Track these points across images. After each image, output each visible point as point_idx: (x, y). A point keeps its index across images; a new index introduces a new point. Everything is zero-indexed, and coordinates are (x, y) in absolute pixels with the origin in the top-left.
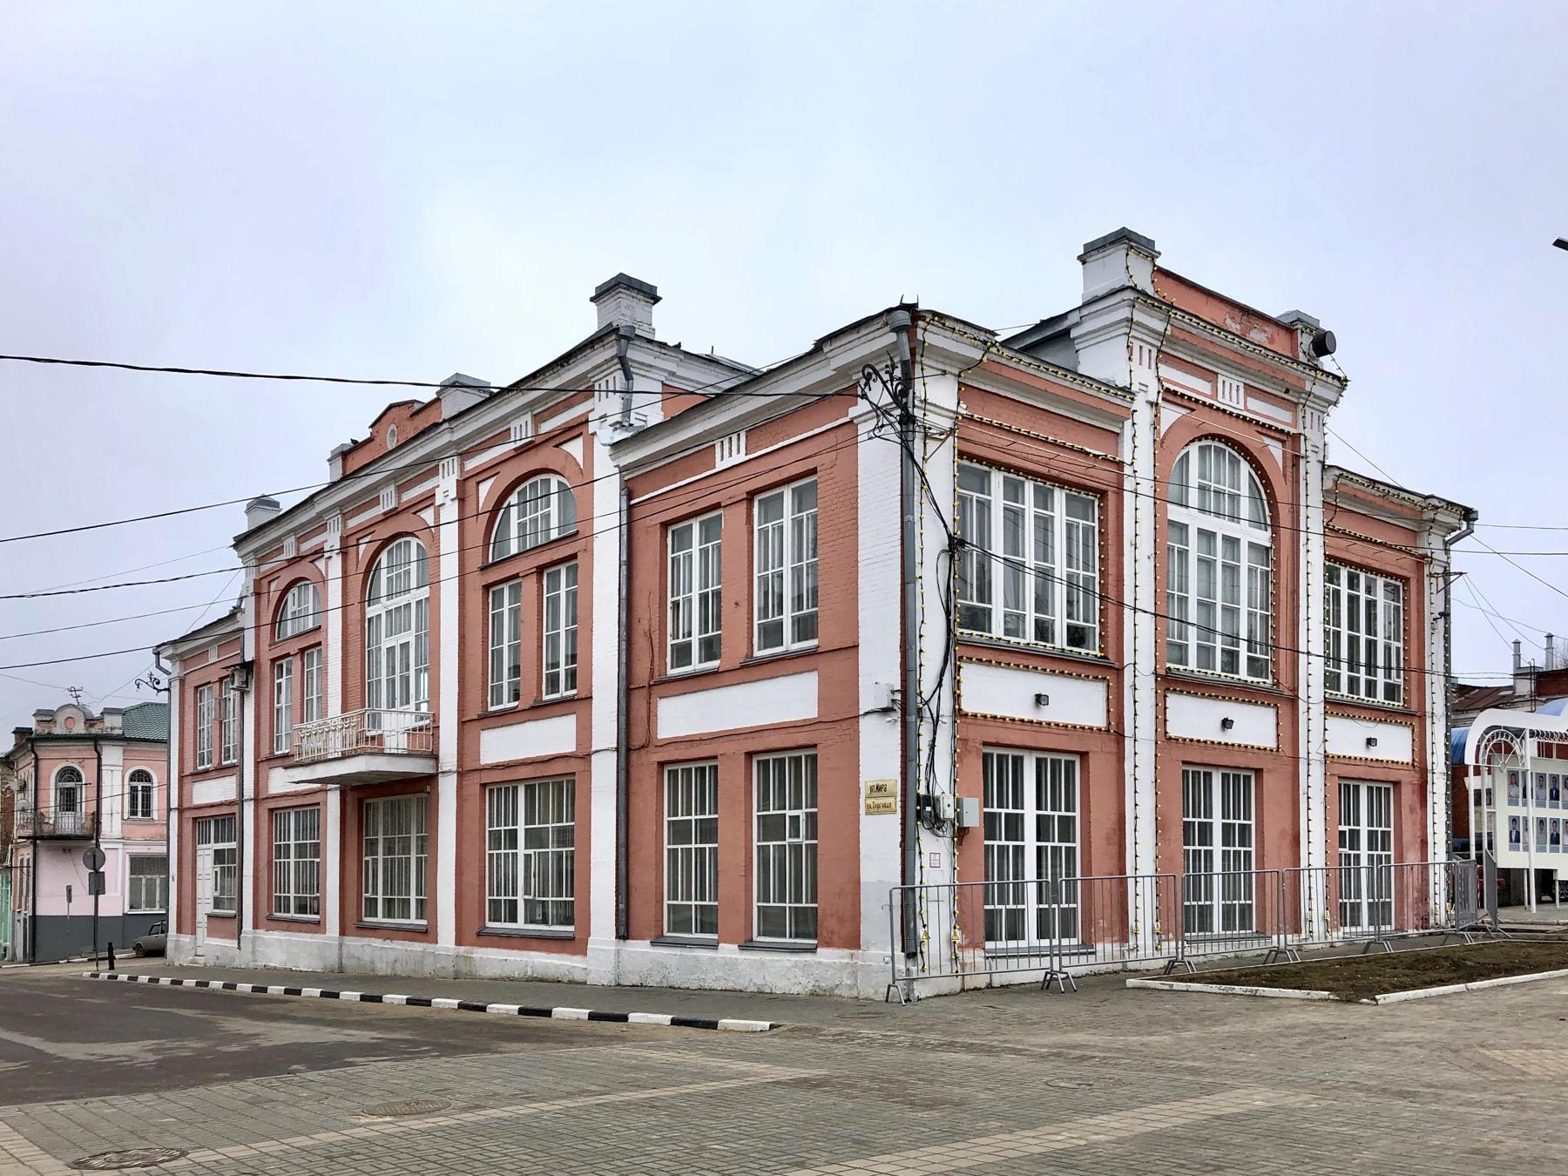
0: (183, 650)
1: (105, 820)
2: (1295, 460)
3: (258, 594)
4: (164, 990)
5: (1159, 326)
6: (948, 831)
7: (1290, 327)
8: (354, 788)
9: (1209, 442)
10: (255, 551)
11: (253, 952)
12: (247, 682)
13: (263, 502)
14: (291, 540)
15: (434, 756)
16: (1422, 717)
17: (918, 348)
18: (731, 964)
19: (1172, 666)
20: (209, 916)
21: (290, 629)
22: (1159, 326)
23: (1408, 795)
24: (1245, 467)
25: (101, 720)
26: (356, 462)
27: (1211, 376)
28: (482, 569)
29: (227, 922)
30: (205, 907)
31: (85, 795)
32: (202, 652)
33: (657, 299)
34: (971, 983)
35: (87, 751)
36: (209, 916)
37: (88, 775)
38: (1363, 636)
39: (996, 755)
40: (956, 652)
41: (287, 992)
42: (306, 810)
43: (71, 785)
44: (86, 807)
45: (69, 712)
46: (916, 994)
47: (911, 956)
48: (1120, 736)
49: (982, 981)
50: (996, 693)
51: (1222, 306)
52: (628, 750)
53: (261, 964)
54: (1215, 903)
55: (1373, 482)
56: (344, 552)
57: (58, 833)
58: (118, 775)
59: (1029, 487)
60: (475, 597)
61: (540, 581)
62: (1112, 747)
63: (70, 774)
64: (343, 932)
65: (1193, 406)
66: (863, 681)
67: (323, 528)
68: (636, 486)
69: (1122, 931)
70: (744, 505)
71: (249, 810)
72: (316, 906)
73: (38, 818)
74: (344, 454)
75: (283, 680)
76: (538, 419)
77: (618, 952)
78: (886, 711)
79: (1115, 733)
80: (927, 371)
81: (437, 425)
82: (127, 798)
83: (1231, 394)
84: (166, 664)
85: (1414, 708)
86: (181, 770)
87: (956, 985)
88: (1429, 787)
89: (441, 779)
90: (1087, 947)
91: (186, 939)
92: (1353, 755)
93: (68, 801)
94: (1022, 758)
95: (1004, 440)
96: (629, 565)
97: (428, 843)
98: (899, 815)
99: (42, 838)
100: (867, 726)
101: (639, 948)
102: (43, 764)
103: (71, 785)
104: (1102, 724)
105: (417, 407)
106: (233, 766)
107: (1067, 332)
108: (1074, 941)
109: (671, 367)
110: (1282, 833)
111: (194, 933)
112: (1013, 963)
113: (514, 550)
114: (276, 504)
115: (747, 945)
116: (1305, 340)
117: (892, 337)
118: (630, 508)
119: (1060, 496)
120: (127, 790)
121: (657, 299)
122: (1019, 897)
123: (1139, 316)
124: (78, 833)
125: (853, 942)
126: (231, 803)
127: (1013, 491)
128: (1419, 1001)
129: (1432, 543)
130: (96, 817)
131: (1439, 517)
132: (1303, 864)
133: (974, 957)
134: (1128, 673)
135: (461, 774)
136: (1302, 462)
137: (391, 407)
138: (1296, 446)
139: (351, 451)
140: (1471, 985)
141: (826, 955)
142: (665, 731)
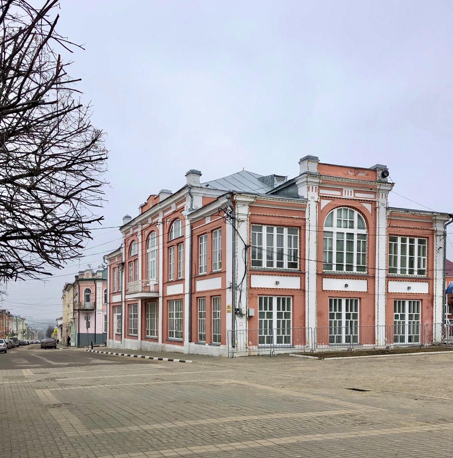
0: (110, 257)
1: (97, 305)
2: (375, 209)
3: (125, 243)
4: (100, 355)
5: (318, 181)
6: (244, 317)
7: (374, 170)
8: (144, 300)
9: (341, 208)
10: (124, 231)
11: (124, 345)
12: (123, 268)
13: (127, 217)
14: (131, 230)
15: (158, 292)
16: (433, 279)
17: (234, 202)
18: (207, 348)
19: (324, 271)
20: (116, 334)
21: (132, 254)
22: (318, 181)
23: (425, 303)
24: (356, 213)
25: (96, 274)
26: (145, 209)
27: (341, 190)
28: (168, 242)
29: (119, 336)
30: (115, 332)
31: (92, 297)
32: (114, 258)
33: (201, 175)
34: (252, 354)
35: (92, 283)
36: (116, 334)
37: (93, 291)
38: (408, 256)
39: (263, 298)
40: (249, 273)
41: (159, 359)
42: (131, 305)
43: (88, 294)
44: (92, 301)
45: (87, 272)
46: (235, 356)
47: (234, 347)
48: (304, 291)
49: (256, 354)
50: (261, 282)
51: (347, 169)
52: (191, 294)
53: (125, 348)
54: (406, 335)
55: (407, 211)
56: (163, 223)
57: (85, 308)
58: (101, 291)
59: (275, 229)
60: (166, 249)
61: (178, 247)
62: (303, 294)
63: (88, 291)
64: (142, 340)
65: (334, 199)
66: (227, 281)
67: (158, 215)
68: (194, 225)
69: (304, 341)
70: (210, 233)
71: (123, 304)
72: (136, 331)
73: (80, 304)
74: (142, 207)
75: (131, 268)
76: (177, 205)
77: (189, 346)
78: (230, 288)
79: (303, 290)
80: (239, 206)
81: (157, 204)
82: (104, 298)
83: (348, 194)
84: (106, 261)
85: (430, 276)
86: (110, 292)
87: (247, 354)
88: (434, 301)
89: (159, 299)
90: (293, 346)
91: (111, 341)
92: (403, 292)
93: (88, 299)
94: (272, 298)
95: (265, 218)
96: (192, 246)
97: (158, 317)
98: (231, 313)
99: (81, 310)
100: (228, 291)
101: (193, 344)
102: (80, 287)
103: (88, 294)
104: (299, 288)
105: (156, 196)
106: (120, 292)
107: (295, 183)
108: (289, 344)
109: (204, 192)
110: (369, 316)
111: (113, 339)
112: (263, 349)
113: (174, 239)
114: (130, 217)
115: (210, 344)
116: (380, 173)
117: (227, 200)
118: (192, 231)
119: (286, 230)
120: (104, 296)
121: (201, 175)
122: (340, 332)
123: (309, 180)
124: (90, 308)
125: (225, 344)
126: (120, 302)
127: (270, 230)
128: (334, 360)
129: (439, 227)
130: (95, 303)
131: (437, 218)
132: (376, 325)
133: (255, 348)
134: (307, 274)
135: (163, 297)
136: (377, 209)
137: (150, 196)
138: (375, 205)
139: (144, 206)
140: (360, 357)
141: (222, 347)
142: (198, 289)
